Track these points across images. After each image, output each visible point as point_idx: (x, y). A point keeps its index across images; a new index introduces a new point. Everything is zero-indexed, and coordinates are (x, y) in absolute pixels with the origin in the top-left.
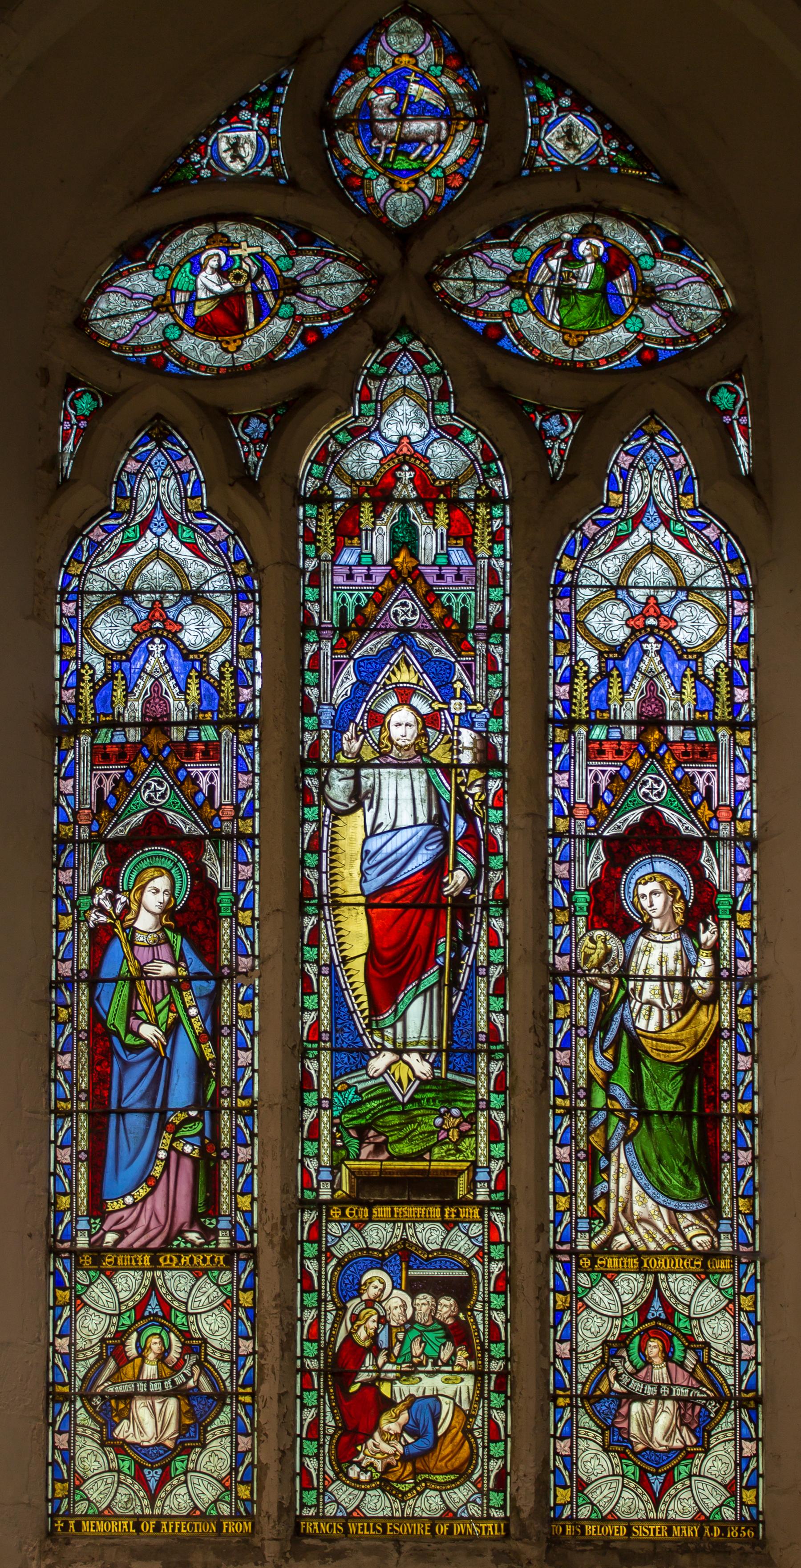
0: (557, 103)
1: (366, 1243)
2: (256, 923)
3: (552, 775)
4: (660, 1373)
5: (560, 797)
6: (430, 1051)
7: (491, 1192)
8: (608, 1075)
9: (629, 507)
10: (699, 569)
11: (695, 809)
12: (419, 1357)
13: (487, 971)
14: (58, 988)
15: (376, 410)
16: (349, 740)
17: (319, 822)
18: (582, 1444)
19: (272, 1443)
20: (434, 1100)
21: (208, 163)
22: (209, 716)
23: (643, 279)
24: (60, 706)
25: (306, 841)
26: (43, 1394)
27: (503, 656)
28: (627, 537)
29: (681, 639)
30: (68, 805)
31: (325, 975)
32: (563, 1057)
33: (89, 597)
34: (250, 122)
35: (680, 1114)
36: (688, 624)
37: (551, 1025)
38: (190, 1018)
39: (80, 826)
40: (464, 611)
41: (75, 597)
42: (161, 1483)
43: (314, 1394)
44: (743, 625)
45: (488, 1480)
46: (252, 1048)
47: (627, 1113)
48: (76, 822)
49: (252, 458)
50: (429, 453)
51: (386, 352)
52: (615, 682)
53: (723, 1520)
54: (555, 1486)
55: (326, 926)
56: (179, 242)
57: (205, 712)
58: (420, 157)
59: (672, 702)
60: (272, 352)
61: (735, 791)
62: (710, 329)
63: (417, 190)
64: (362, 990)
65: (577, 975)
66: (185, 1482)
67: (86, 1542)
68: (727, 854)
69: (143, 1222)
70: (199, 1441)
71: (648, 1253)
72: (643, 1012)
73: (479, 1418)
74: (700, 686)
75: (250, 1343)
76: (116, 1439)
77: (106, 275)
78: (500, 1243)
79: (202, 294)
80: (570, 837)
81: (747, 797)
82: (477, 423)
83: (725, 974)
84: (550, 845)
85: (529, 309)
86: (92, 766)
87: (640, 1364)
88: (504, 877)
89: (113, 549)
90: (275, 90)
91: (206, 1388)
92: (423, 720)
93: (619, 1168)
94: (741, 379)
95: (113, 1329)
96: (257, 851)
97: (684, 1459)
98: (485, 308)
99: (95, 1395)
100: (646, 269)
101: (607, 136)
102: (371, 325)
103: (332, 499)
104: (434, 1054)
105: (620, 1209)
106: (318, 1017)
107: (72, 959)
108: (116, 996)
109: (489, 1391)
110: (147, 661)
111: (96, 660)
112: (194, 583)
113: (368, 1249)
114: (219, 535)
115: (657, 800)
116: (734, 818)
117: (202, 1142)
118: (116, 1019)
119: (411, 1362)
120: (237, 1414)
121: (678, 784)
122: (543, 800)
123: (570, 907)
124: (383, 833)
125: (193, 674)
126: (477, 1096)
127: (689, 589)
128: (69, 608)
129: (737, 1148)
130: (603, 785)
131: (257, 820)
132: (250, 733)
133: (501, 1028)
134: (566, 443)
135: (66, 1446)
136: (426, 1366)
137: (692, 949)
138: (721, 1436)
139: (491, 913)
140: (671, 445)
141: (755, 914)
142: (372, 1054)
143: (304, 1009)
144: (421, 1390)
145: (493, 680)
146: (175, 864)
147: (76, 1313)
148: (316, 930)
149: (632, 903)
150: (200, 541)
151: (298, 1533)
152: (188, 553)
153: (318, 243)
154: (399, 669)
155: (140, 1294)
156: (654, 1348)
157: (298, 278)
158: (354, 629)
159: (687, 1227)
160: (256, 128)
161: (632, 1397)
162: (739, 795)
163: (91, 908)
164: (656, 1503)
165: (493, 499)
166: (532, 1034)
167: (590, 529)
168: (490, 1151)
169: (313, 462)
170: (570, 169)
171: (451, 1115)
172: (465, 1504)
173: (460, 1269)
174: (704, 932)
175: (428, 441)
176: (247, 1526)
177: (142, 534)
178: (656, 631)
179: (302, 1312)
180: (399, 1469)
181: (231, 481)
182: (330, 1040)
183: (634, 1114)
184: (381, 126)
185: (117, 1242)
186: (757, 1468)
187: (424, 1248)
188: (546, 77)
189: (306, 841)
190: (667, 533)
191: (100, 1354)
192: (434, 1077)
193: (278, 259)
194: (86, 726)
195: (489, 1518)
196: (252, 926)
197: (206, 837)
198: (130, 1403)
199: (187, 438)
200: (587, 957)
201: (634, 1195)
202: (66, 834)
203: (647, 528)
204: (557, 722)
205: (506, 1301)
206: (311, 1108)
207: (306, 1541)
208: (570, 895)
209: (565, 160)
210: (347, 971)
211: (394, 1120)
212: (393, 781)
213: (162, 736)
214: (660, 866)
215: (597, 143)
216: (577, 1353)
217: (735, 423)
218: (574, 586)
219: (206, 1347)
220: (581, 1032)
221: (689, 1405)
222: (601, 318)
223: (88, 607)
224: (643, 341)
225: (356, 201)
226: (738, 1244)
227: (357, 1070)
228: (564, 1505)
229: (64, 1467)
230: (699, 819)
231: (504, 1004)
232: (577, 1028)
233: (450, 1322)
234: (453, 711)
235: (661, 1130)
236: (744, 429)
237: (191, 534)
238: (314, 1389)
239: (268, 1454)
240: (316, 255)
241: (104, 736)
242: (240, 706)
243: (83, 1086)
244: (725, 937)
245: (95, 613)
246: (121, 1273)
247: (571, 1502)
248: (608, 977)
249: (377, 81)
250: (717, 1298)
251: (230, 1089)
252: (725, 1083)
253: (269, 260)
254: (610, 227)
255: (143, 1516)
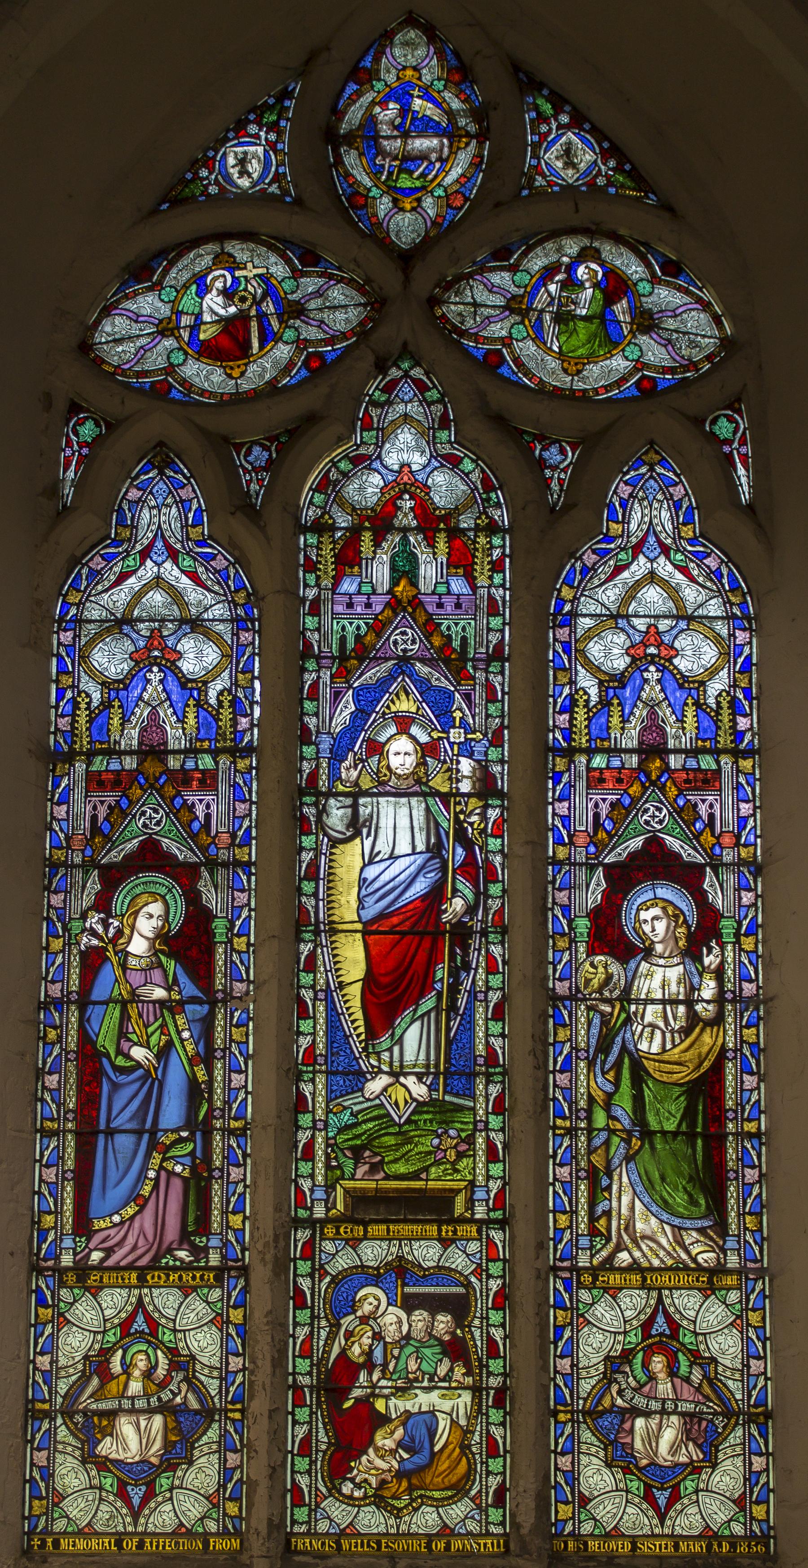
0: (556, 120)
1: (361, 1260)
2: (251, 949)
3: (552, 804)
4: (664, 1388)
5: (560, 826)
6: (428, 1074)
7: (489, 1210)
8: (609, 1096)
9: (628, 537)
10: (700, 597)
11: (697, 836)
12: (415, 1373)
13: (486, 996)
14: (46, 1009)
15: (377, 438)
16: (348, 769)
17: (317, 850)
18: (584, 1460)
19: (263, 1459)
20: (431, 1121)
21: (216, 179)
22: (206, 744)
23: (642, 306)
24: (55, 733)
25: (303, 869)
26: (22, 1411)
27: (502, 685)
28: (627, 566)
29: (682, 667)
30: (61, 830)
31: (321, 1000)
32: (563, 1079)
33: (88, 626)
34: (257, 136)
35: (684, 1133)
36: (689, 653)
37: (551, 1048)
38: (182, 1040)
39: (73, 851)
40: (464, 639)
41: (72, 625)
42: (145, 1501)
43: (306, 1410)
44: (745, 654)
45: (487, 1496)
46: (246, 1071)
47: (629, 1133)
48: (69, 847)
49: (254, 487)
50: (430, 481)
51: (388, 379)
52: (616, 711)
53: (732, 1536)
54: (556, 1501)
55: (322, 952)
56: (186, 262)
57: (202, 741)
58: (423, 175)
59: (674, 730)
60: (275, 378)
61: (738, 817)
62: (709, 358)
63: (419, 210)
64: (359, 1015)
65: (577, 1000)
66: (171, 1499)
67: (64, 1560)
68: (731, 879)
69: (131, 1240)
70: (185, 1458)
71: (652, 1269)
72: (645, 1034)
73: (477, 1433)
74: (702, 715)
75: (240, 1360)
76: (98, 1456)
77: (112, 297)
78: (499, 1260)
79: (207, 318)
80: (570, 864)
81: (751, 823)
82: (477, 452)
83: (729, 996)
84: (550, 872)
85: (529, 335)
86: (86, 792)
87: (644, 1379)
88: (503, 904)
89: (113, 578)
90: (282, 103)
91: (194, 1404)
92: (422, 748)
93: (621, 1186)
94: (740, 409)
95: (97, 1346)
96: (253, 878)
97: (690, 1474)
98: (485, 334)
99: (77, 1412)
100: (644, 296)
101: (605, 155)
102: (373, 351)
103: (333, 528)
104: (431, 1077)
105: (622, 1227)
106: (314, 1041)
107: (62, 981)
108: (107, 1018)
109: (487, 1406)
110: (144, 689)
111: (93, 689)
112: (193, 611)
113: (363, 1266)
114: (220, 563)
115: (658, 827)
116: (737, 844)
117: (193, 1161)
118: (106, 1041)
119: (407, 1378)
120: (226, 1431)
121: (680, 811)
122: (543, 828)
123: (570, 933)
124: (381, 861)
125: (191, 702)
126: (475, 1117)
127: (690, 618)
128: (67, 637)
129: (743, 1166)
130: (604, 813)
131: (254, 848)
132: (247, 762)
133: (500, 1052)
134: (566, 473)
135: (45, 1463)
136: (422, 1381)
137: (695, 972)
138: (729, 1451)
139: (490, 940)
140: (671, 475)
141: (760, 937)
142: (369, 1076)
143: (299, 1033)
144: (417, 1406)
145: (492, 709)
146: (170, 891)
147: (59, 1331)
148: (312, 956)
149: (634, 928)
150: (200, 570)
151: (288, 1549)
152: (188, 581)
153: (323, 264)
154: (398, 698)
155: (126, 1311)
156: (658, 1363)
157: (303, 301)
158: (353, 658)
159: (692, 1244)
160: (264, 143)
161: (635, 1412)
162: (742, 822)
163: (83, 931)
164: (662, 1518)
165: (492, 528)
166: (532, 1057)
167: (590, 558)
168: (488, 1170)
169: (314, 491)
170: (568, 189)
171: (449, 1136)
172: (463, 1520)
173: (457, 1285)
174: (708, 956)
175: (428, 470)
176: (236, 1544)
177: (143, 562)
178: (657, 659)
179: (294, 1328)
180: (394, 1488)
181: (233, 509)
182: (326, 1063)
183: (636, 1134)
184: (386, 143)
185: (103, 1260)
186: (768, 1483)
187: (420, 1266)
188: (545, 92)
189: (303, 869)
190: (667, 563)
191: (83, 1371)
192: (431, 1099)
193: (283, 280)
194: (81, 753)
195: (488, 1534)
196: (248, 952)
197: (201, 864)
198: (114, 1420)
199: (189, 466)
200: (588, 981)
201: (637, 1212)
202: (59, 859)
203: (647, 557)
204: (557, 751)
205: (504, 1318)
206: (306, 1129)
207: (297, 1558)
208: (570, 922)
209: (563, 179)
210: (343, 996)
211: (390, 1140)
212: (391, 809)
213: (159, 764)
214: (662, 892)
215: (595, 162)
216: (578, 1369)
217: (735, 452)
218: (574, 615)
219: (194, 1364)
220: (583, 1054)
221: (696, 1420)
222: (600, 346)
223: (86, 636)
224: (641, 370)
225: (360, 220)
226: (746, 1260)
227: (353, 1092)
228: (565, 1521)
229: (42, 1485)
230: (701, 846)
231: (503, 1028)
232: (578, 1051)
233: (447, 1338)
234: (452, 740)
235: (665, 1149)
236: (744, 458)
237: (192, 563)
238: (306, 1405)
239: (258, 1471)
240: (320, 277)
241: (99, 763)
242: (238, 734)
243: (71, 1106)
244: (730, 960)
245: (92, 642)
246: (106, 1291)
247: (573, 1518)
248: (609, 1001)
249: (382, 95)
250: (724, 1314)
251: (223, 1110)
252: (730, 1103)
253: (275, 282)
254: (608, 250)
255: (126, 1533)
